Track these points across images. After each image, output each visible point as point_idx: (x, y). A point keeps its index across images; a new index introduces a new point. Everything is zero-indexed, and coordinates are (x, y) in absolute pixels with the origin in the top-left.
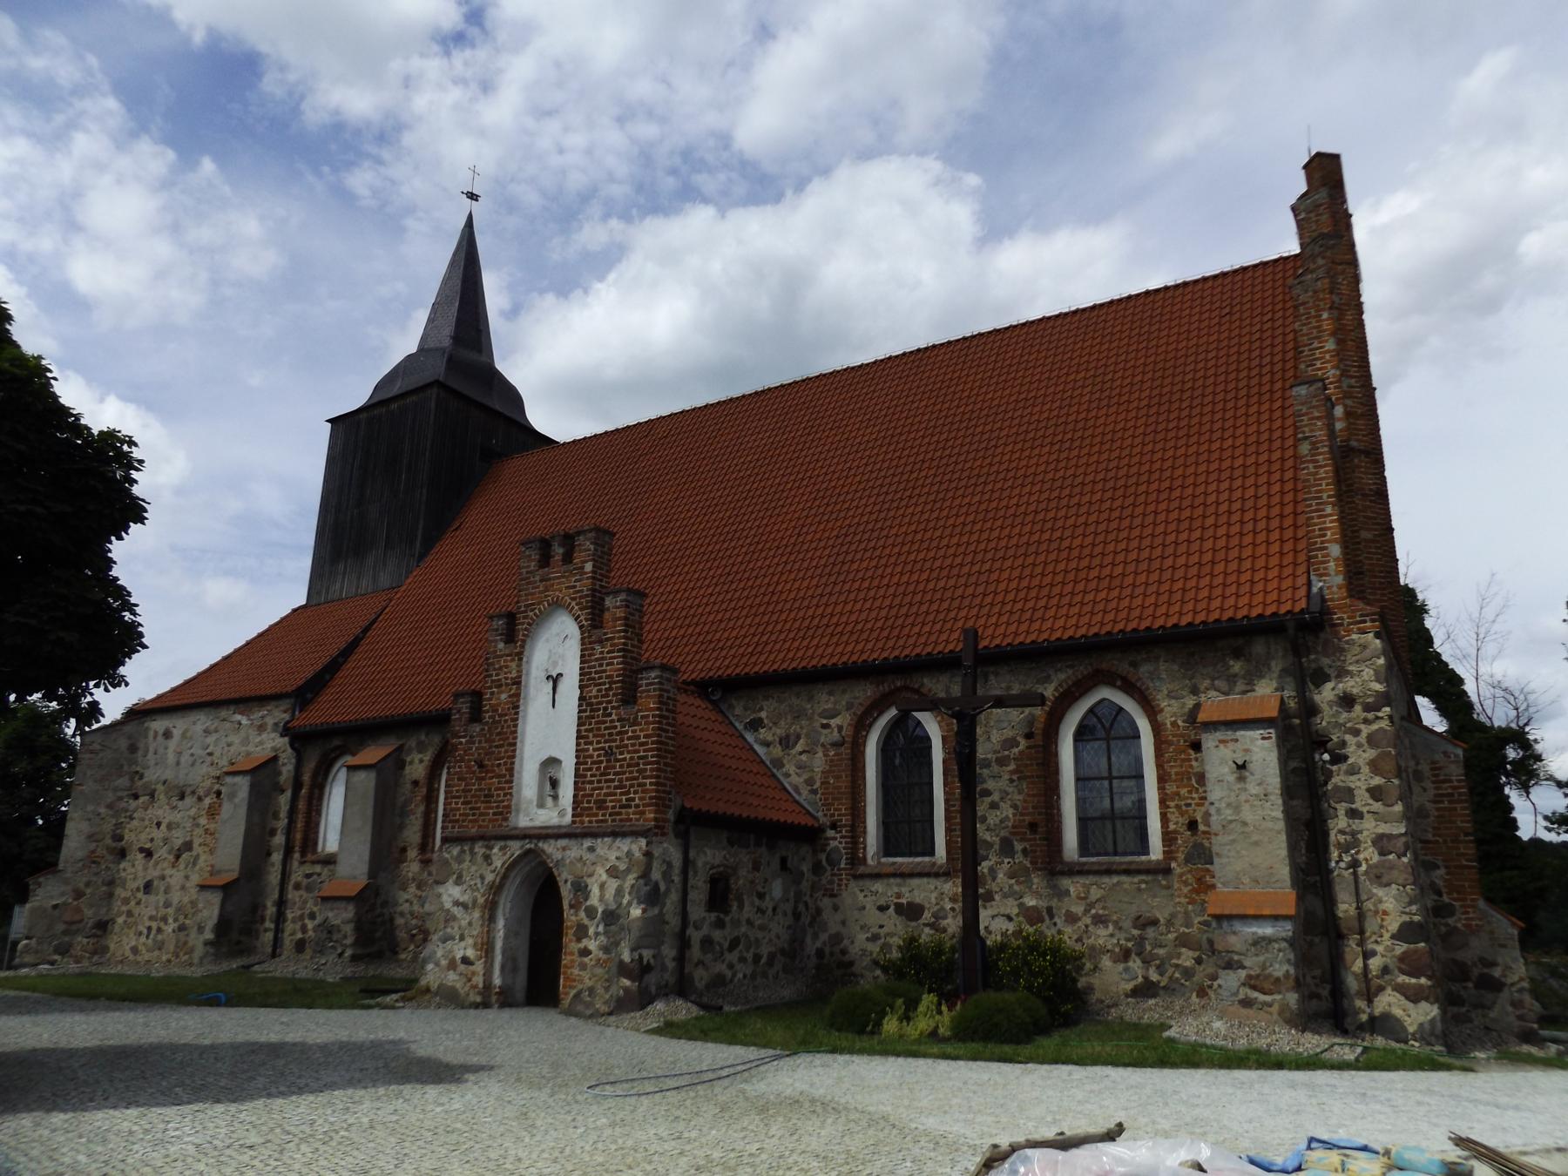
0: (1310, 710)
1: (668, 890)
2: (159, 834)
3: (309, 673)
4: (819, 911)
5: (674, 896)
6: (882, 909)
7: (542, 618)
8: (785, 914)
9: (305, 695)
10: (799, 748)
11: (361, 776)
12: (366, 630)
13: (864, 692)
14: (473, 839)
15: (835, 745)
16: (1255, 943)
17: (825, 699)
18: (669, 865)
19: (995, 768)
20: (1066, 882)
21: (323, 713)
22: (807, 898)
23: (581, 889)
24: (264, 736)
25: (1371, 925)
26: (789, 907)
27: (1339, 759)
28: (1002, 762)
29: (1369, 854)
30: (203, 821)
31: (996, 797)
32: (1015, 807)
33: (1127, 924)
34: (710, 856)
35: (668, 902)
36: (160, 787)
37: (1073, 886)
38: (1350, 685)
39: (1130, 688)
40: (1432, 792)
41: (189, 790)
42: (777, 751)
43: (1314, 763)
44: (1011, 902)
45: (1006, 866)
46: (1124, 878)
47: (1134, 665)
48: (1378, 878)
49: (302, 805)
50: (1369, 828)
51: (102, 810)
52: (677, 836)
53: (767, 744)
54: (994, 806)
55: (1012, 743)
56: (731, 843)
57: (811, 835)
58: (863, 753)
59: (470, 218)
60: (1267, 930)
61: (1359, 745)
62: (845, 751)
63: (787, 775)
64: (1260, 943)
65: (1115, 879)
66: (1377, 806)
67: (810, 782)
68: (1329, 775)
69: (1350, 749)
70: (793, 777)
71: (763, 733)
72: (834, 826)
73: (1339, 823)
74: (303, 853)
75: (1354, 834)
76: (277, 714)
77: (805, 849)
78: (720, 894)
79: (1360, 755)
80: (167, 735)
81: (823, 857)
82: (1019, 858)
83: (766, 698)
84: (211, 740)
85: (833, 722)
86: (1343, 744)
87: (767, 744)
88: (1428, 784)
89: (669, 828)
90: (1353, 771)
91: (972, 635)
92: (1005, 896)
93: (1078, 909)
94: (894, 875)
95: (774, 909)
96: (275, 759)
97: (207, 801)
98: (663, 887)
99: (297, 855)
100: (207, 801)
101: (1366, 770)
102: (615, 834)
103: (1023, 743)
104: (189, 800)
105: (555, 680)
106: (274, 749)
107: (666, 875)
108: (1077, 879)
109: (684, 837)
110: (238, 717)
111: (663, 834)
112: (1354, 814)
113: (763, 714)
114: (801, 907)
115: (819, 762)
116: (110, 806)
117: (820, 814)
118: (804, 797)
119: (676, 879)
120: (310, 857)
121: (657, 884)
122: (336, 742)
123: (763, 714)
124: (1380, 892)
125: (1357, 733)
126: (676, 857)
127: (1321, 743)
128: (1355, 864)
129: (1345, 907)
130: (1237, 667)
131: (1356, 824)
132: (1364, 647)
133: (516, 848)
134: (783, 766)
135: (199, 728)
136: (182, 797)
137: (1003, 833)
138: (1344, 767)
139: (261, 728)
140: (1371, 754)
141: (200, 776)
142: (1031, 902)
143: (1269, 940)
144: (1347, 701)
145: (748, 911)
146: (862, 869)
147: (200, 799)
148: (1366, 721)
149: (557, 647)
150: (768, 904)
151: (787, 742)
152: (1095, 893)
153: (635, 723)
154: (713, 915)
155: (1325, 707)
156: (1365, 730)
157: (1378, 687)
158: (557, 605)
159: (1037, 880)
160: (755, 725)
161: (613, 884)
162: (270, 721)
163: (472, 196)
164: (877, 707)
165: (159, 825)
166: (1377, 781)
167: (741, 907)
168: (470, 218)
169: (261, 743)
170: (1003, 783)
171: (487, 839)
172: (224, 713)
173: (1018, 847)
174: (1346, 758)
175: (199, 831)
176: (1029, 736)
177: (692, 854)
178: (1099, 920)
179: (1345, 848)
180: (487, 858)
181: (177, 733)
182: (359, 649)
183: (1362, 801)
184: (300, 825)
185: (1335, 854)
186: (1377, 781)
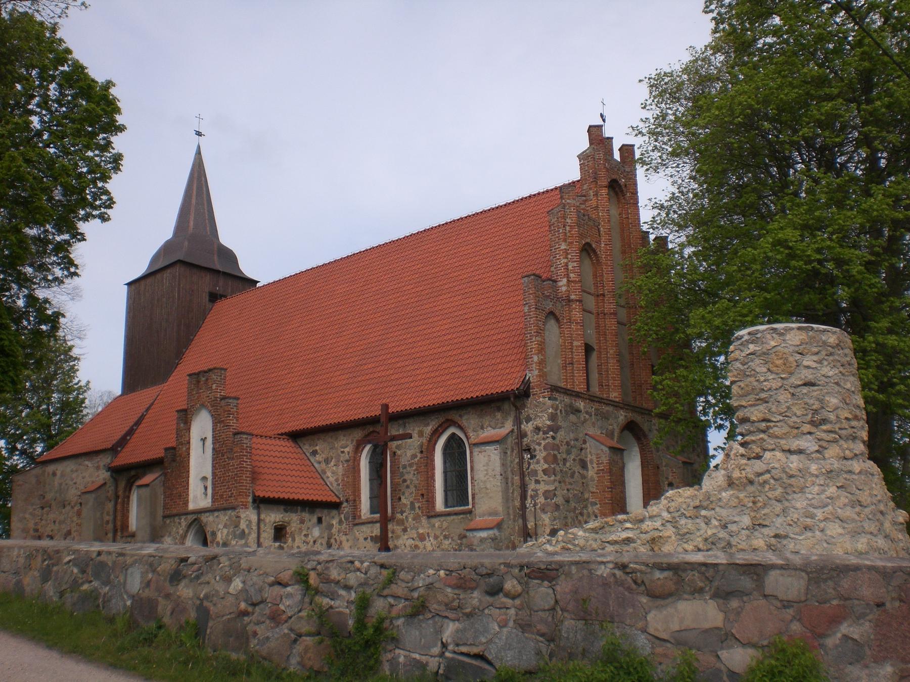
0: (522, 435)
1: (250, 533)
2: (56, 527)
3: (118, 436)
4: (341, 543)
5: (254, 535)
6: (366, 539)
7: (198, 410)
8: (322, 544)
9: (114, 450)
10: (332, 464)
11: (143, 490)
12: (152, 404)
13: (358, 434)
14: (174, 516)
15: (347, 461)
16: (481, 541)
17: (414, 429)
18: (250, 522)
19: (408, 469)
20: (434, 520)
21: (127, 457)
22: (336, 536)
23: (214, 534)
24: (100, 472)
25: (540, 531)
26: (324, 542)
27: (533, 457)
28: (411, 465)
29: (541, 500)
30: (75, 519)
31: (408, 482)
32: (415, 487)
33: (456, 538)
34: (273, 517)
35: (250, 538)
36: (53, 503)
37: (437, 522)
38: (538, 422)
39: (461, 428)
40: (596, 469)
41: (66, 503)
42: (323, 465)
43: (523, 458)
44: (414, 531)
45: (412, 515)
46: (454, 517)
47: (461, 416)
48: (543, 510)
49: (119, 507)
50: (542, 488)
51: (27, 516)
52: (254, 508)
53: (319, 463)
54: (408, 487)
55: (414, 456)
56: (286, 511)
57: (336, 506)
58: (359, 465)
59: (199, 147)
60: (484, 534)
61: (540, 450)
62: (351, 463)
63: (328, 477)
64: (482, 540)
65: (452, 517)
66: (545, 478)
67: (337, 480)
68: (529, 464)
69: (537, 452)
70: (331, 478)
71: (318, 458)
72: (347, 501)
73: (532, 486)
74: (122, 532)
75: (536, 491)
76: (106, 460)
77: (334, 512)
78: (280, 532)
79: (541, 455)
80: (54, 474)
81: (342, 516)
82: (417, 510)
83: (318, 439)
84: (74, 475)
85: (346, 450)
86: (535, 450)
87: (319, 463)
88: (595, 465)
89: (250, 505)
90: (538, 462)
91: (386, 407)
92: (412, 529)
93: (438, 533)
94: (369, 523)
95: (315, 542)
96: (105, 484)
97: (76, 508)
98: (247, 531)
99: (119, 534)
100: (76, 508)
101: (542, 461)
102: (225, 509)
103: (419, 455)
104: (68, 508)
105: (204, 440)
106: (104, 479)
107: (249, 525)
108: (438, 519)
109: (258, 508)
110: (87, 463)
111: (246, 508)
112: (537, 482)
113: (317, 448)
114: (332, 541)
115: (340, 470)
116: (31, 514)
117: (341, 496)
118: (334, 487)
119: (255, 528)
120: (126, 534)
121: (243, 530)
122: (133, 473)
123: (317, 448)
124: (543, 516)
125: (539, 444)
126: (254, 518)
127: (528, 450)
128: (535, 505)
129: (531, 525)
130: (499, 415)
131: (538, 486)
132: (544, 404)
133: (191, 518)
134: (325, 473)
135: (68, 470)
136: (64, 507)
137: (411, 500)
138: (535, 460)
139: (98, 468)
140: (544, 454)
141: (72, 494)
142: (421, 531)
143: (486, 539)
144: (537, 429)
145: (298, 541)
146: (357, 521)
147: (72, 507)
148: (544, 439)
149: (202, 426)
150: (310, 539)
151: (327, 461)
152: (445, 525)
153: (233, 459)
154: (277, 544)
155: (529, 433)
156: (543, 443)
157: (548, 423)
158: (203, 406)
159: (424, 520)
160: (315, 453)
161: (225, 531)
162: (102, 464)
163: (199, 134)
164: (436, 434)
165: (54, 522)
166: (546, 466)
167: (294, 540)
168: (199, 147)
169: (98, 476)
170: (411, 476)
171: (179, 515)
172: (80, 460)
173: (417, 505)
174: (535, 456)
175: (74, 524)
176: (422, 452)
177: (262, 516)
178: (446, 537)
179: (531, 496)
180: (180, 523)
181: (58, 473)
182: (144, 421)
183: (541, 476)
184: (119, 518)
185: (529, 500)
186: (546, 466)
